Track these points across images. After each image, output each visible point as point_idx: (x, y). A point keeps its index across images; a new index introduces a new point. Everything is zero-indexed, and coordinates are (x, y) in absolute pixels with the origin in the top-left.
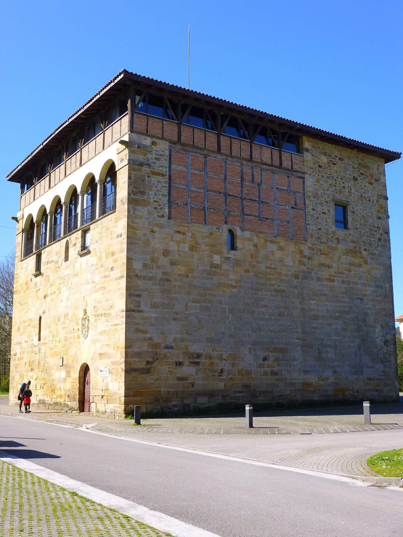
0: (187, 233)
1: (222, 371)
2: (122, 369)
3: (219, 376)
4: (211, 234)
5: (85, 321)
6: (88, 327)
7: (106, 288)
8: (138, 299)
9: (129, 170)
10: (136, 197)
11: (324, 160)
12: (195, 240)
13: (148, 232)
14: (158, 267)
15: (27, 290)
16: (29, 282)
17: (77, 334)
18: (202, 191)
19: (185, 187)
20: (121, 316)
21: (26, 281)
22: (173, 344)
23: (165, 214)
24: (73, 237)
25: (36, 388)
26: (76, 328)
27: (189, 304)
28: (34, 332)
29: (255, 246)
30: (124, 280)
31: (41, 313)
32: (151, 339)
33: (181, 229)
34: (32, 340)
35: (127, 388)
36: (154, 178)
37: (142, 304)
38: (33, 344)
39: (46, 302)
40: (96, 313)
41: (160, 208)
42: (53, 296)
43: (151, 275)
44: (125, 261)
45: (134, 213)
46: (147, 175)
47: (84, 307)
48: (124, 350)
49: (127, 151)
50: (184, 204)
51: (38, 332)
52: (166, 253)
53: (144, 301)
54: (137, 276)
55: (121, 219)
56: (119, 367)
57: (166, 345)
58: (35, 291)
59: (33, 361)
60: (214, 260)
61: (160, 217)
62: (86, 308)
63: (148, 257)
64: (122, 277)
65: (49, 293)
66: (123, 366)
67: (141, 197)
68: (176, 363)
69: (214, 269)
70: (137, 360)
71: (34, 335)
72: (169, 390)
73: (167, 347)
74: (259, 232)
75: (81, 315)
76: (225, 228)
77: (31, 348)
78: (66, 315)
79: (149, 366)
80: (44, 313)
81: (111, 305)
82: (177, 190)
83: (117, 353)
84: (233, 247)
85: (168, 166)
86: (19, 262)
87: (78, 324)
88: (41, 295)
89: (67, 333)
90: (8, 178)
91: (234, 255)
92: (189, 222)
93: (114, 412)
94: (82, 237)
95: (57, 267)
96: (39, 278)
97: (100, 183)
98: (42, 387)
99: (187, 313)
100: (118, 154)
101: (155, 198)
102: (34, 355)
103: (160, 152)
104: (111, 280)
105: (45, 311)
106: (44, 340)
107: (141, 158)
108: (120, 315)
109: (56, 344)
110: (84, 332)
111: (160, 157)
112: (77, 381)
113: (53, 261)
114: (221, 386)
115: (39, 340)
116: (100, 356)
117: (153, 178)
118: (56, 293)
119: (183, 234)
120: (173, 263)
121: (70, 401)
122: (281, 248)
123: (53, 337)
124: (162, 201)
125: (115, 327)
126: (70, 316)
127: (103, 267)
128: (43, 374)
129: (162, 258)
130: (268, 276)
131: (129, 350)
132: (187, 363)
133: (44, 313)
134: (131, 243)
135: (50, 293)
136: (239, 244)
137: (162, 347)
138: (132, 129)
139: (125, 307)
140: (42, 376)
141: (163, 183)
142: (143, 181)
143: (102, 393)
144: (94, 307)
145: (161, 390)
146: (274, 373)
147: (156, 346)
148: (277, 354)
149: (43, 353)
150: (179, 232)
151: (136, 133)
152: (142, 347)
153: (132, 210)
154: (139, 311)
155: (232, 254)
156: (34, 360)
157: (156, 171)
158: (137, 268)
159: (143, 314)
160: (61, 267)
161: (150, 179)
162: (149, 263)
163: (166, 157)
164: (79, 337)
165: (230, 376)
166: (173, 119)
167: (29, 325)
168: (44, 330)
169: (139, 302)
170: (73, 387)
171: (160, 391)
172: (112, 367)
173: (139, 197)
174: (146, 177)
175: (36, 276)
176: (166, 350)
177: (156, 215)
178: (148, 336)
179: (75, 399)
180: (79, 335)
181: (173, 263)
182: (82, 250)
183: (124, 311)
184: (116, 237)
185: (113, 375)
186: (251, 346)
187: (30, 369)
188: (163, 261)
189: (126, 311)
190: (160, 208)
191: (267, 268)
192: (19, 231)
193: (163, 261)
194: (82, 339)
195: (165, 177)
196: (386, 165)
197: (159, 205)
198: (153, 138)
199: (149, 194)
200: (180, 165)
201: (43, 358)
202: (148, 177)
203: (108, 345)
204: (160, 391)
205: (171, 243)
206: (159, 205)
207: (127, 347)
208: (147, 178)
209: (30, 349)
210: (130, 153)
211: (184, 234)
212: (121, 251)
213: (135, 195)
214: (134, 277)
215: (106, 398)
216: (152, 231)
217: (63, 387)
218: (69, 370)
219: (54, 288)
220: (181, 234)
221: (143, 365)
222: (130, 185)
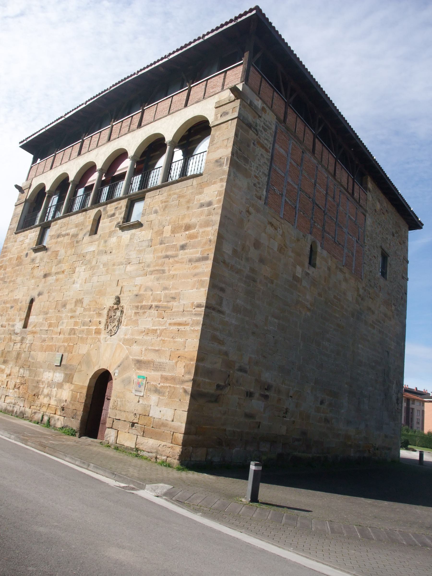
0: (279, 229)
1: (287, 412)
2: (185, 391)
3: (283, 417)
4: (298, 240)
5: (115, 313)
6: (120, 322)
7: (167, 271)
8: (221, 294)
9: (237, 125)
10: (239, 161)
11: (378, 206)
12: (284, 240)
13: (244, 211)
14: (247, 259)
15: (18, 266)
16: (23, 258)
17: (96, 328)
18: (296, 187)
19: (283, 175)
20: (194, 313)
21: (18, 256)
22: (248, 367)
23: (262, 196)
24: (111, 208)
25: (7, 386)
26: (96, 319)
27: (269, 318)
28: (19, 316)
29: (329, 269)
30: (209, 263)
31: (34, 294)
32: (226, 354)
33: (274, 221)
34: (13, 326)
35: (189, 422)
36: (258, 148)
37: (224, 303)
38: (14, 330)
39: (45, 282)
40: (139, 304)
41: (259, 187)
42: (61, 276)
43: (239, 267)
44: (214, 238)
45: (234, 180)
46: (253, 141)
47: (117, 294)
48: (194, 363)
49: (238, 102)
50: (280, 194)
51: (25, 317)
52: (257, 245)
53: (227, 300)
54: (224, 262)
55: (213, 184)
56: (179, 388)
57: (240, 366)
58: (31, 268)
59: (9, 352)
60: (296, 272)
61: (257, 197)
62: (120, 296)
63: (239, 243)
64: (205, 259)
65: (54, 270)
66: (189, 387)
67: (244, 164)
68: (247, 393)
69: (295, 283)
70: (207, 380)
71: (18, 320)
72: (235, 430)
73: (242, 370)
74: (334, 256)
75: (110, 302)
76: (310, 237)
77: (10, 335)
78: (79, 302)
79: (219, 392)
80: (40, 294)
81: (173, 296)
82: (276, 175)
83: (176, 365)
84: (312, 263)
85: (272, 143)
86: (12, 234)
87: (99, 315)
88: (39, 273)
89: (76, 324)
90: (21, 144)
91: (313, 272)
92: (282, 217)
93: (157, 452)
94: (127, 207)
95: (74, 241)
96: (40, 254)
97: (172, 144)
98: (17, 386)
99: (266, 328)
100: (216, 108)
101: (256, 173)
102: (12, 344)
103: (268, 123)
104: (177, 262)
105: (42, 293)
106: (33, 327)
107: (250, 118)
108: (192, 311)
109: (52, 336)
110: (110, 328)
111: (267, 129)
112: (85, 391)
113: (68, 234)
114: (283, 430)
115: (25, 326)
116: (137, 365)
117: (258, 148)
118: (65, 273)
119: (275, 228)
120: (262, 261)
121: (64, 415)
122: (346, 280)
123: (50, 325)
124: (262, 180)
125: (177, 327)
126: (86, 302)
127: (164, 244)
128: (22, 371)
129: (252, 249)
130: (334, 306)
131: (201, 364)
132: (257, 395)
133: (40, 294)
134: (226, 216)
135: (56, 272)
136: (318, 261)
137: (236, 368)
138: (246, 79)
139: (205, 302)
140: (20, 373)
141: (265, 159)
142: (248, 146)
143: (132, 418)
144: (137, 295)
145: (227, 429)
146: (327, 421)
147: (229, 364)
148: (331, 398)
149: (28, 345)
150: (271, 224)
151: (250, 87)
152: (216, 363)
153: (232, 174)
154: (220, 312)
155: (311, 271)
156: (11, 349)
157: (261, 141)
158: (227, 252)
159: (223, 316)
160: (81, 242)
161: (255, 147)
162: (239, 250)
163: (272, 132)
164: (98, 332)
165: (293, 419)
166: (281, 93)
167: (12, 307)
168: (36, 315)
169: (221, 299)
170: (74, 398)
171: (225, 430)
172: (162, 384)
173: (241, 163)
174: (252, 143)
175: (36, 250)
176: (240, 374)
177: (254, 194)
178: (224, 348)
179: (75, 414)
180: (100, 329)
181: (262, 261)
182: (123, 222)
183: (202, 307)
184: (198, 205)
185: (163, 396)
186: (313, 385)
187: (3, 360)
188: (253, 253)
189: (207, 307)
190: (259, 187)
191: (335, 297)
192: (19, 202)
193: (253, 253)
194: (104, 335)
195: (268, 154)
196: (410, 232)
197: (259, 183)
198: (264, 104)
199: (252, 164)
200: (282, 148)
201: (26, 350)
202: (254, 144)
203: (158, 351)
204: (225, 430)
205: (263, 234)
206: (259, 183)
207: (200, 359)
208: (252, 145)
209: (8, 336)
210: (241, 106)
211: (276, 229)
212: (207, 224)
213: (238, 159)
214: (222, 263)
215: (141, 427)
216: (248, 211)
217: (55, 394)
218: (71, 374)
219: (65, 266)
220: (274, 228)
221: (211, 390)
222: (235, 143)
